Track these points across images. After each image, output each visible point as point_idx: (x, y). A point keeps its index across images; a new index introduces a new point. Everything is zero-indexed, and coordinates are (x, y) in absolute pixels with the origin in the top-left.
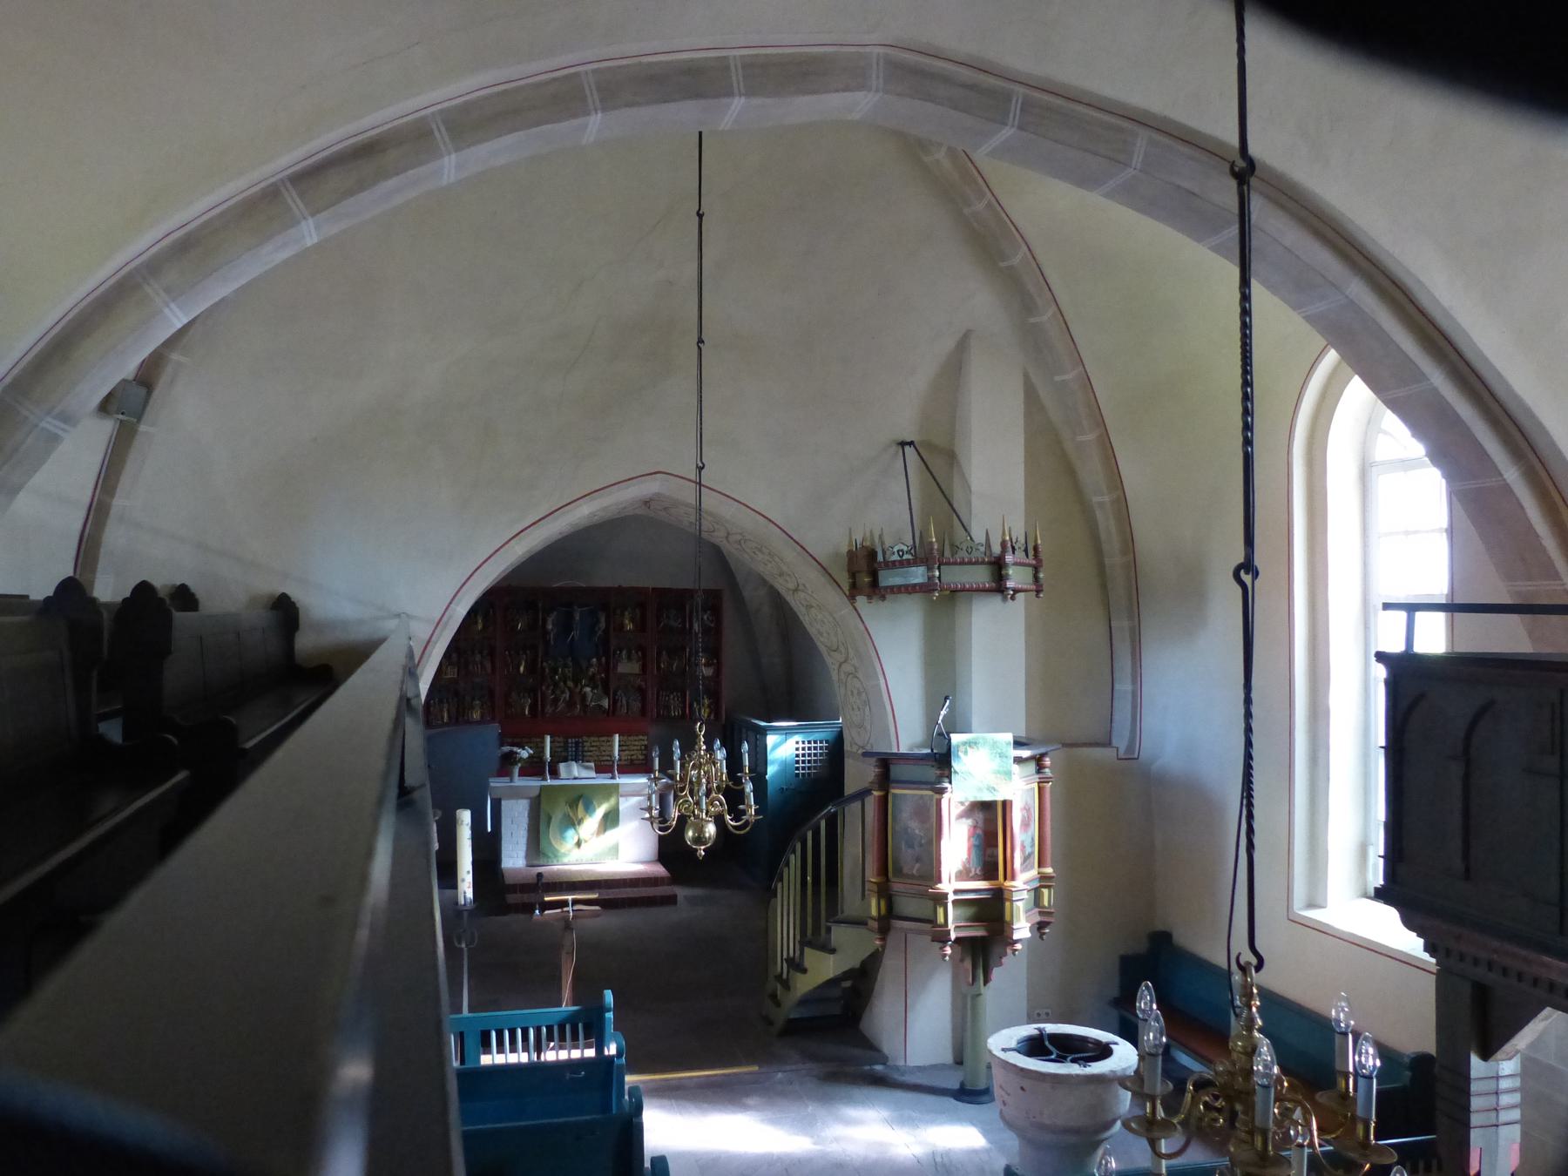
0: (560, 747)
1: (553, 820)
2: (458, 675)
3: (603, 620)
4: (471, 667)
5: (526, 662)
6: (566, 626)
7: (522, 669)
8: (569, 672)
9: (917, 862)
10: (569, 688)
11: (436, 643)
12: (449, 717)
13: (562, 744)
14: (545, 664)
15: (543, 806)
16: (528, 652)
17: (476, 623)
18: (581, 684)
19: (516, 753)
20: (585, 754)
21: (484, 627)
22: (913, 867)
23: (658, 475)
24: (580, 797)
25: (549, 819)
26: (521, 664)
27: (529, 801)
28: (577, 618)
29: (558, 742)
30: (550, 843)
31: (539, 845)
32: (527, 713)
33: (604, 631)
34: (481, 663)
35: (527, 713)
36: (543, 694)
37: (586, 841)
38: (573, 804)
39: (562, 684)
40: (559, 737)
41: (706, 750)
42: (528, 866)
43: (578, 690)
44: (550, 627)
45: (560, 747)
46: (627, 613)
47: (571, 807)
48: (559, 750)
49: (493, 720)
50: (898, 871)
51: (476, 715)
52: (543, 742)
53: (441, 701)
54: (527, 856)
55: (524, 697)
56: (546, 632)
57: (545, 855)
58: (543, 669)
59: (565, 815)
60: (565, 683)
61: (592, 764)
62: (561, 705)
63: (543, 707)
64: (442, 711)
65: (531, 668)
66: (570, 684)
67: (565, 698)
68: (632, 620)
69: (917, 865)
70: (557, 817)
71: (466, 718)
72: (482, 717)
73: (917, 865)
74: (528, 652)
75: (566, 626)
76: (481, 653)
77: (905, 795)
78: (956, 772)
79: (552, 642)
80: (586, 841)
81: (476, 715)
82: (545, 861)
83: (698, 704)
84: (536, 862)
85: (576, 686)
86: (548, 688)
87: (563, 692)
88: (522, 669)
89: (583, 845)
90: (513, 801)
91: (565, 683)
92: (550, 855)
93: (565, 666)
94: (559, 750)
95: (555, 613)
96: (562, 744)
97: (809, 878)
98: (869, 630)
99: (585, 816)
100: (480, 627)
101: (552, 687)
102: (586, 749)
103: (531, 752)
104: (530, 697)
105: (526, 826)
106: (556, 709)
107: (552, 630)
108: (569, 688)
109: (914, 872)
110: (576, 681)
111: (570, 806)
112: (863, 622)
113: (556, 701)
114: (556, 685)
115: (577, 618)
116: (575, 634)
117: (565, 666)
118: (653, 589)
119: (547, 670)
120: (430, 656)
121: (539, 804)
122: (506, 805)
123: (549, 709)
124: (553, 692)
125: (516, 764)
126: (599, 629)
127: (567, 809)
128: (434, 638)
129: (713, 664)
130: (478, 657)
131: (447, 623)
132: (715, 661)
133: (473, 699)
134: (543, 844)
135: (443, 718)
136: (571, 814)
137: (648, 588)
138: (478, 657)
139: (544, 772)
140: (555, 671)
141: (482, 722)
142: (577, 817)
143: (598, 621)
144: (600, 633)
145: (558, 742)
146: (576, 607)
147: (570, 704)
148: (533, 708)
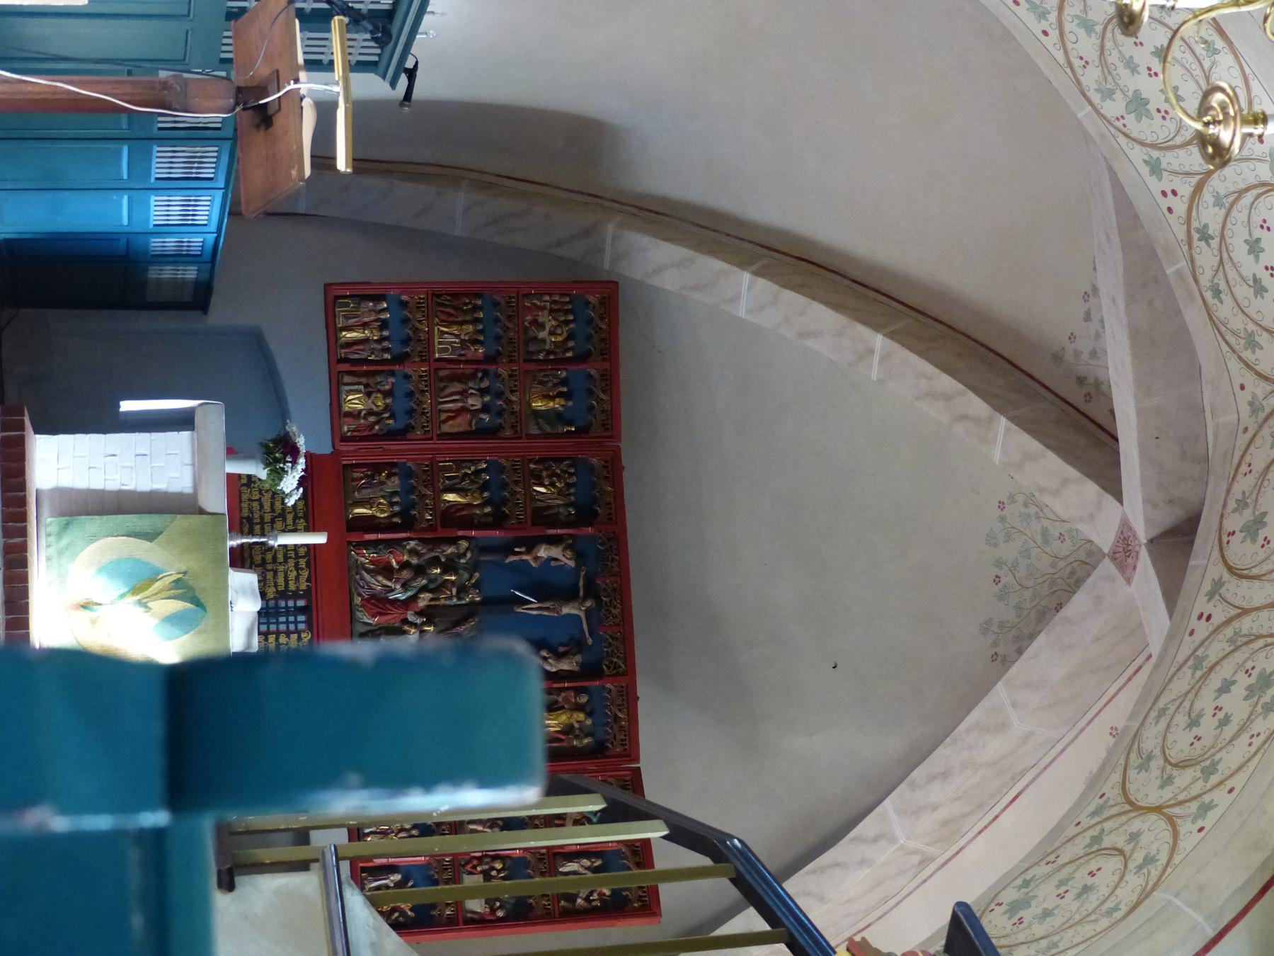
0: (286, 581)
5: (469, 505)
7: (451, 497)
8: (449, 599)
10: (414, 598)
12: (350, 344)
13: (292, 587)
14: (464, 544)
15: (181, 521)
16: (488, 510)
17: (547, 397)
19: (294, 462)
21: (536, 414)
25: (150, 536)
26: (462, 496)
29: (297, 578)
30: (93, 538)
31: (88, 514)
32: (357, 511)
34: (463, 410)
35: (357, 511)
36: (398, 543)
37: (94, 622)
38: (184, 589)
39: (424, 582)
40: (308, 580)
41: (576, 704)
43: (411, 617)
44: (543, 552)
45: (286, 581)
48: (281, 580)
49: (339, 437)
51: (354, 401)
52: (310, 529)
53: (384, 325)
54: (60, 492)
56: (531, 544)
58: (453, 541)
60: (424, 589)
62: (378, 583)
64: (365, 325)
65: (452, 517)
66: (424, 600)
67: (392, 590)
72: (355, 415)
74: (488, 510)
76: (485, 408)
79: (512, 558)
81: (354, 401)
84: (46, 510)
85: (419, 613)
86: (413, 552)
87: (405, 586)
88: (451, 497)
91: (424, 589)
92: (65, 541)
93: (462, 590)
94: (281, 580)
95: (572, 564)
97: (532, 843)
100: (538, 405)
101: (414, 561)
103: (290, 502)
105: (131, 486)
106: (369, 571)
107: (536, 558)
108: (414, 598)
110: (430, 614)
111: (177, 581)
113: (387, 571)
114: (420, 571)
118: (637, 771)
119: (450, 550)
122: (181, 440)
123: (366, 557)
124: (404, 565)
130: (474, 402)
132: (500, 914)
133: (387, 394)
134: (93, 524)
136: (158, 585)
138: (474, 402)
139: (242, 533)
140: (449, 567)
141: (337, 412)
145: (297, 578)
146: (588, 604)
148: (368, 524)
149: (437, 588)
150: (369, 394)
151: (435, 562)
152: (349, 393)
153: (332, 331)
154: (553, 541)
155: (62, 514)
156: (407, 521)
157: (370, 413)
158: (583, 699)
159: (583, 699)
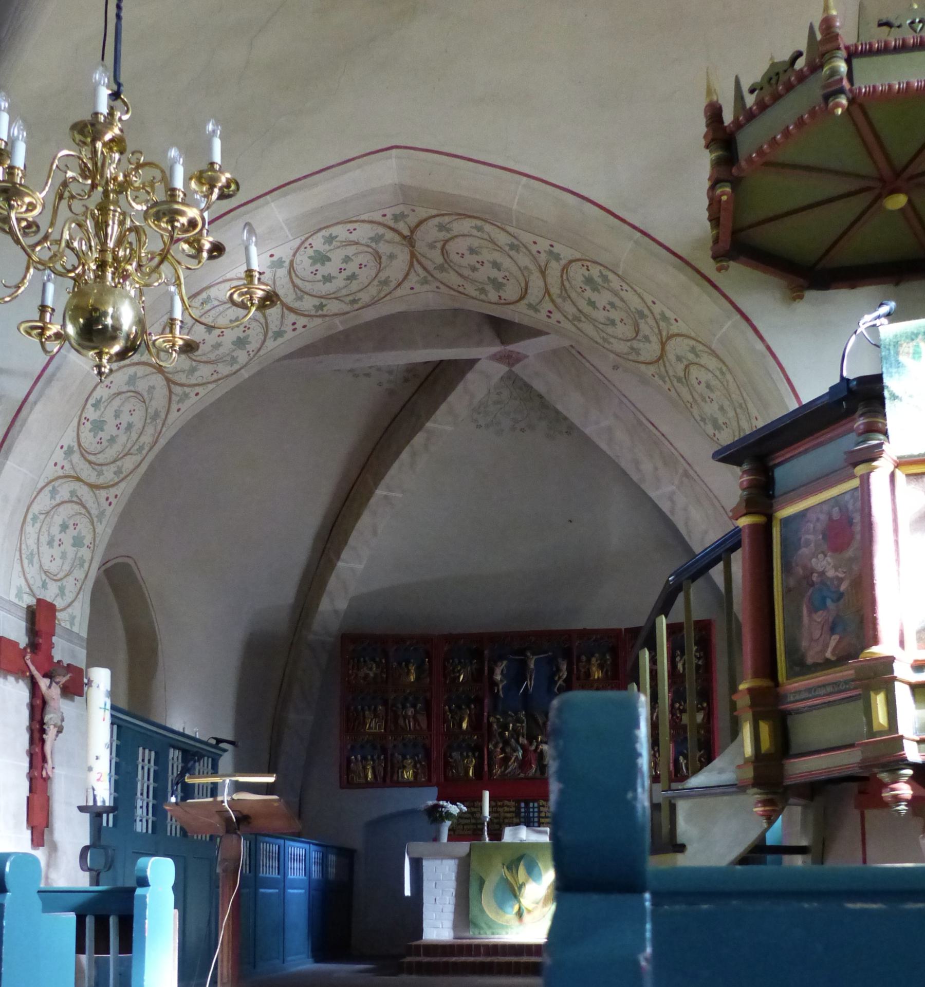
0: (510, 812)
1: (486, 883)
2: (385, 729)
3: (564, 667)
4: (401, 722)
5: (470, 716)
6: (518, 674)
7: (464, 725)
8: (523, 727)
9: (832, 630)
11: (35, 403)
13: (513, 809)
15: (474, 864)
17: (408, 673)
18: (537, 741)
19: (442, 807)
20: (542, 820)
22: (826, 646)
23: (394, 151)
24: (519, 859)
27: (457, 861)
28: (532, 666)
30: (482, 911)
32: (471, 774)
33: (565, 681)
34: (414, 718)
35: (471, 774)
38: (513, 866)
40: (509, 801)
42: (455, 938)
43: (533, 748)
44: (498, 677)
45: (510, 812)
46: (594, 660)
47: (509, 868)
48: (509, 815)
49: (428, 783)
50: (799, 666)
51: (408, 775)
52: (480, 799)
53: (364, 758)
54: (455, 927)
55: (468, 757)
56: (494, 684)
57: (476, 925)
58: (490, 725)
59: (502, 878)
60: (517, 741)
61: (548, 829)
62: (513, 765)
63: (491, 766)
64: (364, 768)
65: (476, 725)
67: (517, 757)
68: (601, 667)
69: (835, 639)
70: (491, 883)
71: (395, 778)
72: (416, 775)
73: (835, 639)
75: (518, 674)
76: (414, 706)
77: (803, 514)
78: (894, 397)
80: (529, 911)
81: (408, 775)
82: (476, 932)
83: (686, 757)
84: (466, 934)
85: (531, 743)
86: (496, 746)
87: (515, 750)
88: (464, 725)
89: (526, 916)
90: (438, 862)
91: (517, 741)
92: (483, 925)
93: (519, 720)
95: (505, 663)
96: (513, 809)
98: (774, 349)
99: (527, 881)
101: (501, 745)
102: (543, 815)
103: (465, 809)
104: (474, 756)
107: (501, 681)
108: (523, 747)
109: (828, 655)
111: (507, 868)
112: (761, 338)
113: (506, 760)
114: (506, 743)
115: (532, 666)
116: (529, 684)
117: (519, 720)
120: (22, 426)
121: (469, 866)
122: (428, 866)
123: (497, 770)
124: (503, 750)
125: (443, 821)
126: (560, 678)
127: (505, 872)
128: (32, 398)
129: (703, 709)
130: (410, 712)
131: (53, 375)
132: (705, 705)
133: (404, 758)
134: (474, 911)
135: (366, 777)
137: (621, 630)
138: (410, 712)
142: (516, 881)
143: (559, 670)
144: (560, 682)
146: (529, 654)
147: (524, 764)
148: (478, 769)
149: (516, 734)
150: (404, 767)
151: (502, 735)
152: (403, 776)
153: (368, 785)
154: (492, 672)
155: (468, 927)
156: (477, 749)
157: (415, 767)
158: (584, 658)
159: (584, 658)
